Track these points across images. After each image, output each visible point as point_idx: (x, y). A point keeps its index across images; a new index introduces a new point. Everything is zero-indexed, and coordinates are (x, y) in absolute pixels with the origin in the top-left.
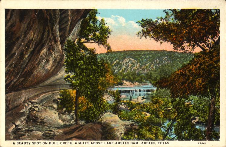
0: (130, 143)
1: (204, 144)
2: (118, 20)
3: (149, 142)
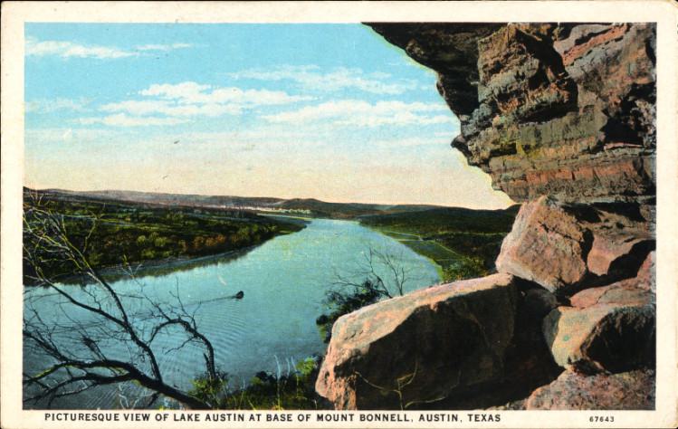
0: (121, 417)
1: (607, 420)
2: (439, 55)
3: (443, 415)
